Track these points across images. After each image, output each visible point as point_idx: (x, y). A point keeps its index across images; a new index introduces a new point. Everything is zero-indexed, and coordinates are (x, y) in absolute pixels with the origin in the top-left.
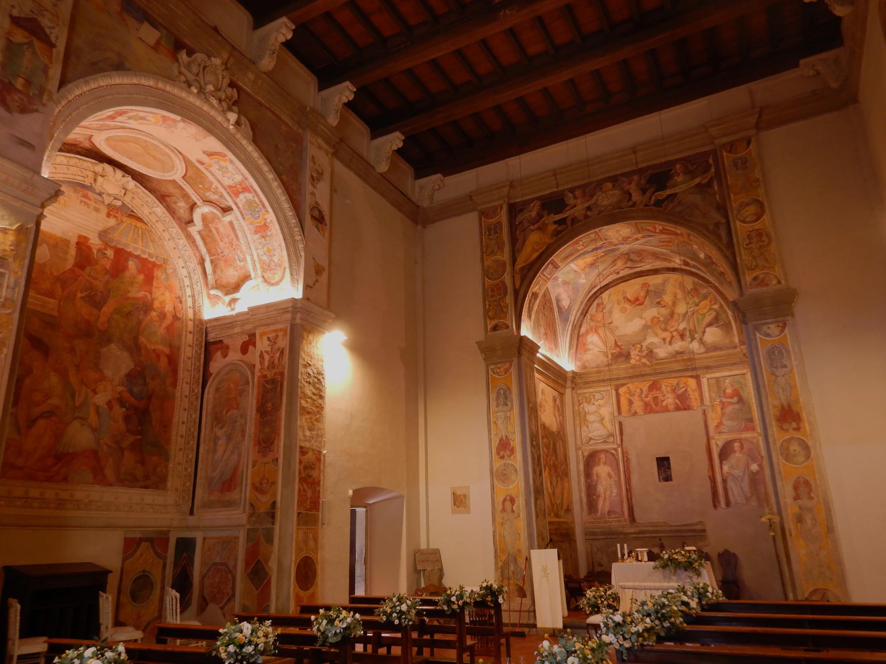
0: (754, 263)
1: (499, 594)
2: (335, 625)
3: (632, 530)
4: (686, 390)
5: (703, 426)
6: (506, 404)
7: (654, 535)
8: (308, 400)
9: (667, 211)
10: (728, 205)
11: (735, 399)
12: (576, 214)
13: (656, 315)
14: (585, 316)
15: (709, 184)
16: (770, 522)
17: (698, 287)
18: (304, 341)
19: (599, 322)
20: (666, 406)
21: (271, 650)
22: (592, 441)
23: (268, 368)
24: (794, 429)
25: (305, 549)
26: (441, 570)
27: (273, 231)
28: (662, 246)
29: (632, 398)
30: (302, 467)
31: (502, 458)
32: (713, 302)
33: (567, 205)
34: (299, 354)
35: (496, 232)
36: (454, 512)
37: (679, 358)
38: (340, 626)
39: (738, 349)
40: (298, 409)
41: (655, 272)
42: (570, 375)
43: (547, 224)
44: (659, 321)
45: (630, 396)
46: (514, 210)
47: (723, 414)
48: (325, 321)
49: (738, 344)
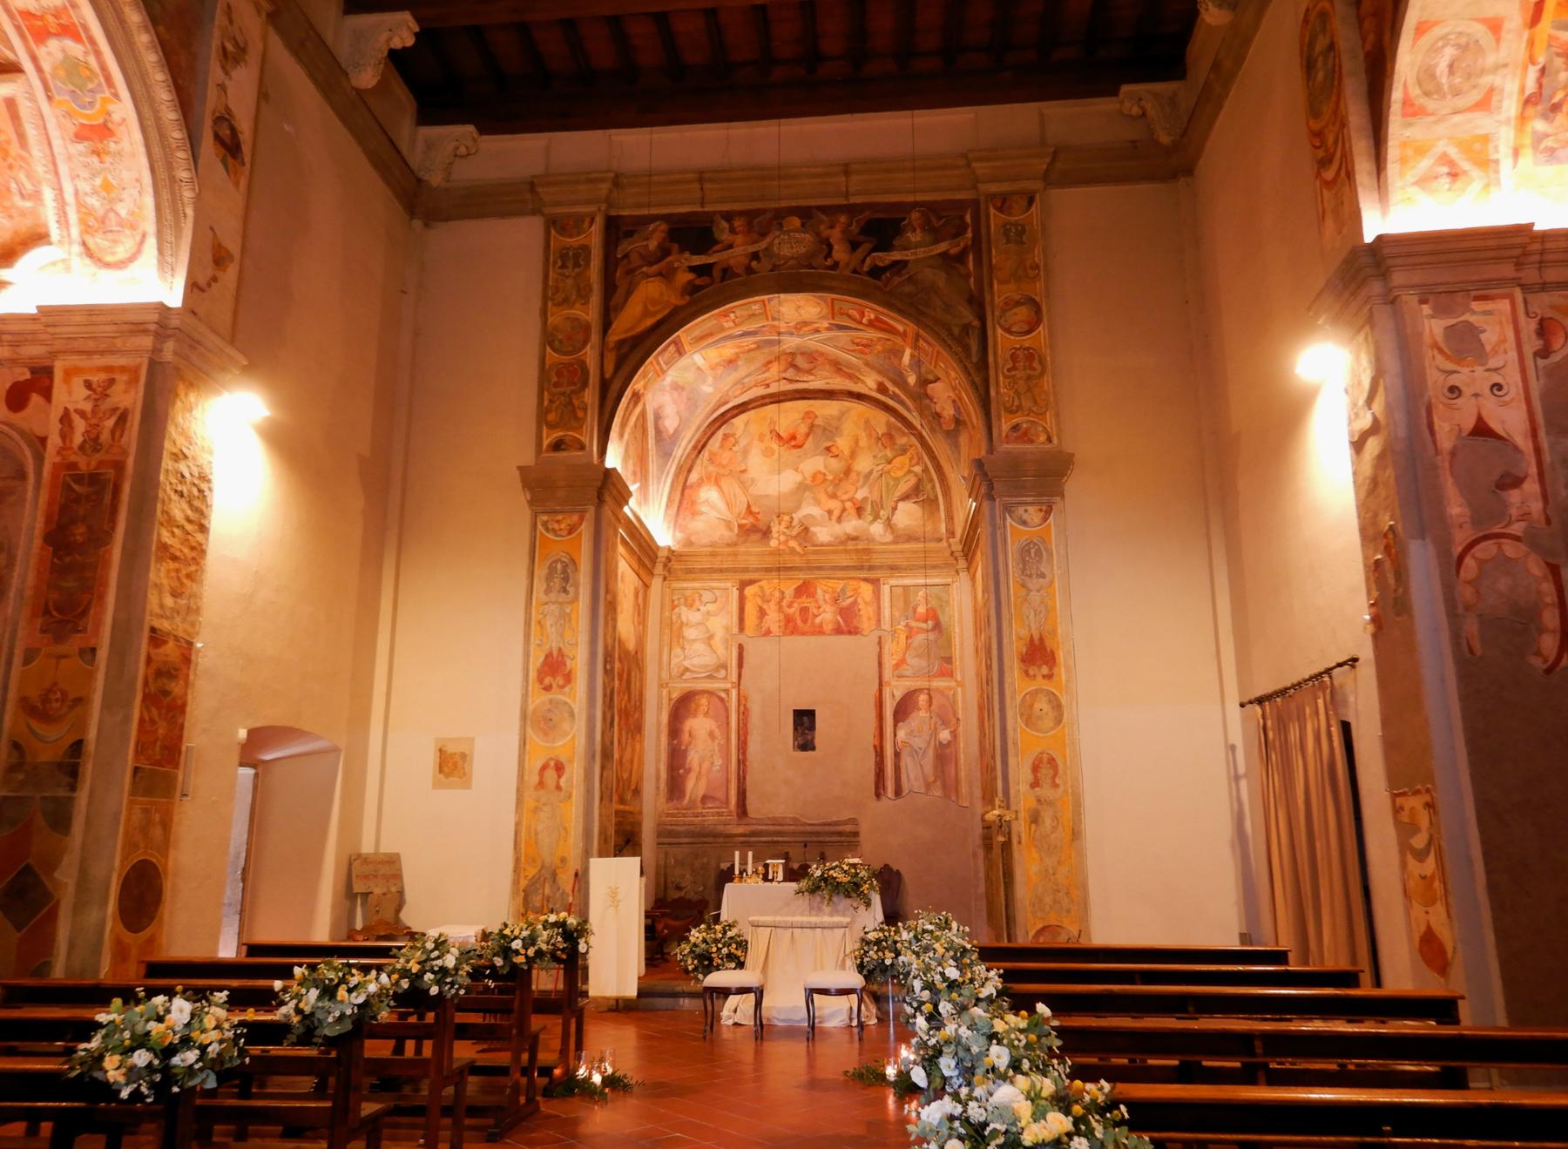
0: (1016, 403)
1: (580, 936)
2: (339, 998)
3: (741, 830)
4: (855, 602)
5: (876, 664)
6: (565, 591)
7: (775, 839)
8: (176, 530)
9: (887, 289)
10: (988, 297)
11: (930, 623)
12: (732, 262)
13: (821, 468)
14: (700, 452)
15: (961, 258)
16: (1000, 820)
17: (893, 433)
18: (179, 404)
19: (724, 467)
20: (821, 626)
21: (231, 1057)
22: (688, 674)
23: (81, 447)
24: (1044, 677)
25: (142, 845)
26: (401, 893)
27: (125, 145)
28: (853, 351)
29: (765, 607)
30: (151, 671)
31: (548, 688)
32: (914, 461)
33: (717, 242)
34: (164, 428)
35: (577, 265)
36: (437, 785)
37: (851, 546)
38: (349, 1001)
39: (944, 544)
40: (154, 548)
41: (829, 394)
42: (662, 554)
43: (677, 269)
44: (825, 480)
45: (763, 601)
46: (616, 229)
47: (908, 646)
48: (224, 369)
49: (944, 536)
